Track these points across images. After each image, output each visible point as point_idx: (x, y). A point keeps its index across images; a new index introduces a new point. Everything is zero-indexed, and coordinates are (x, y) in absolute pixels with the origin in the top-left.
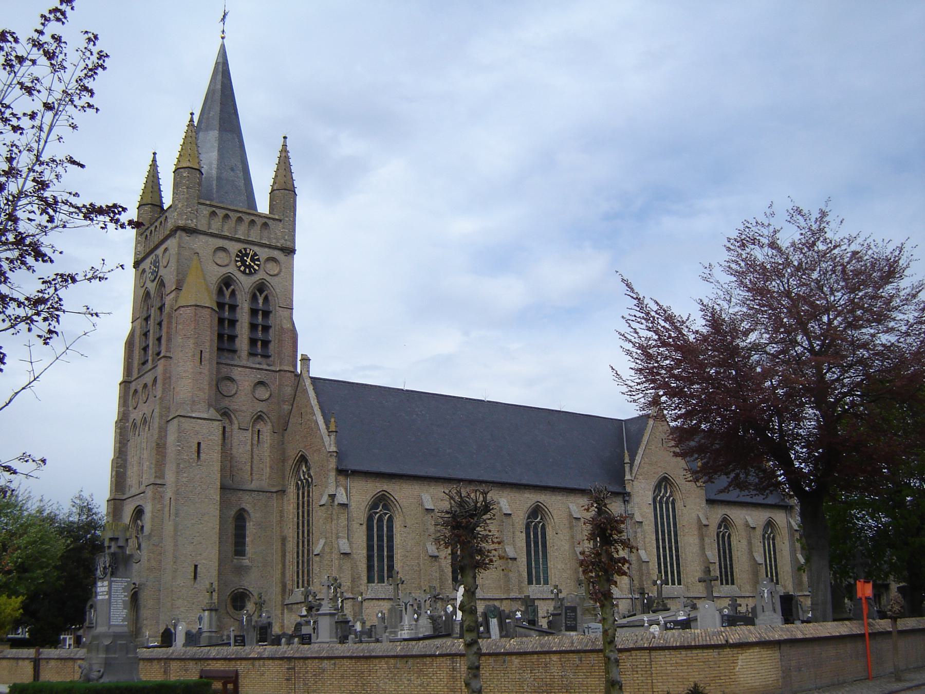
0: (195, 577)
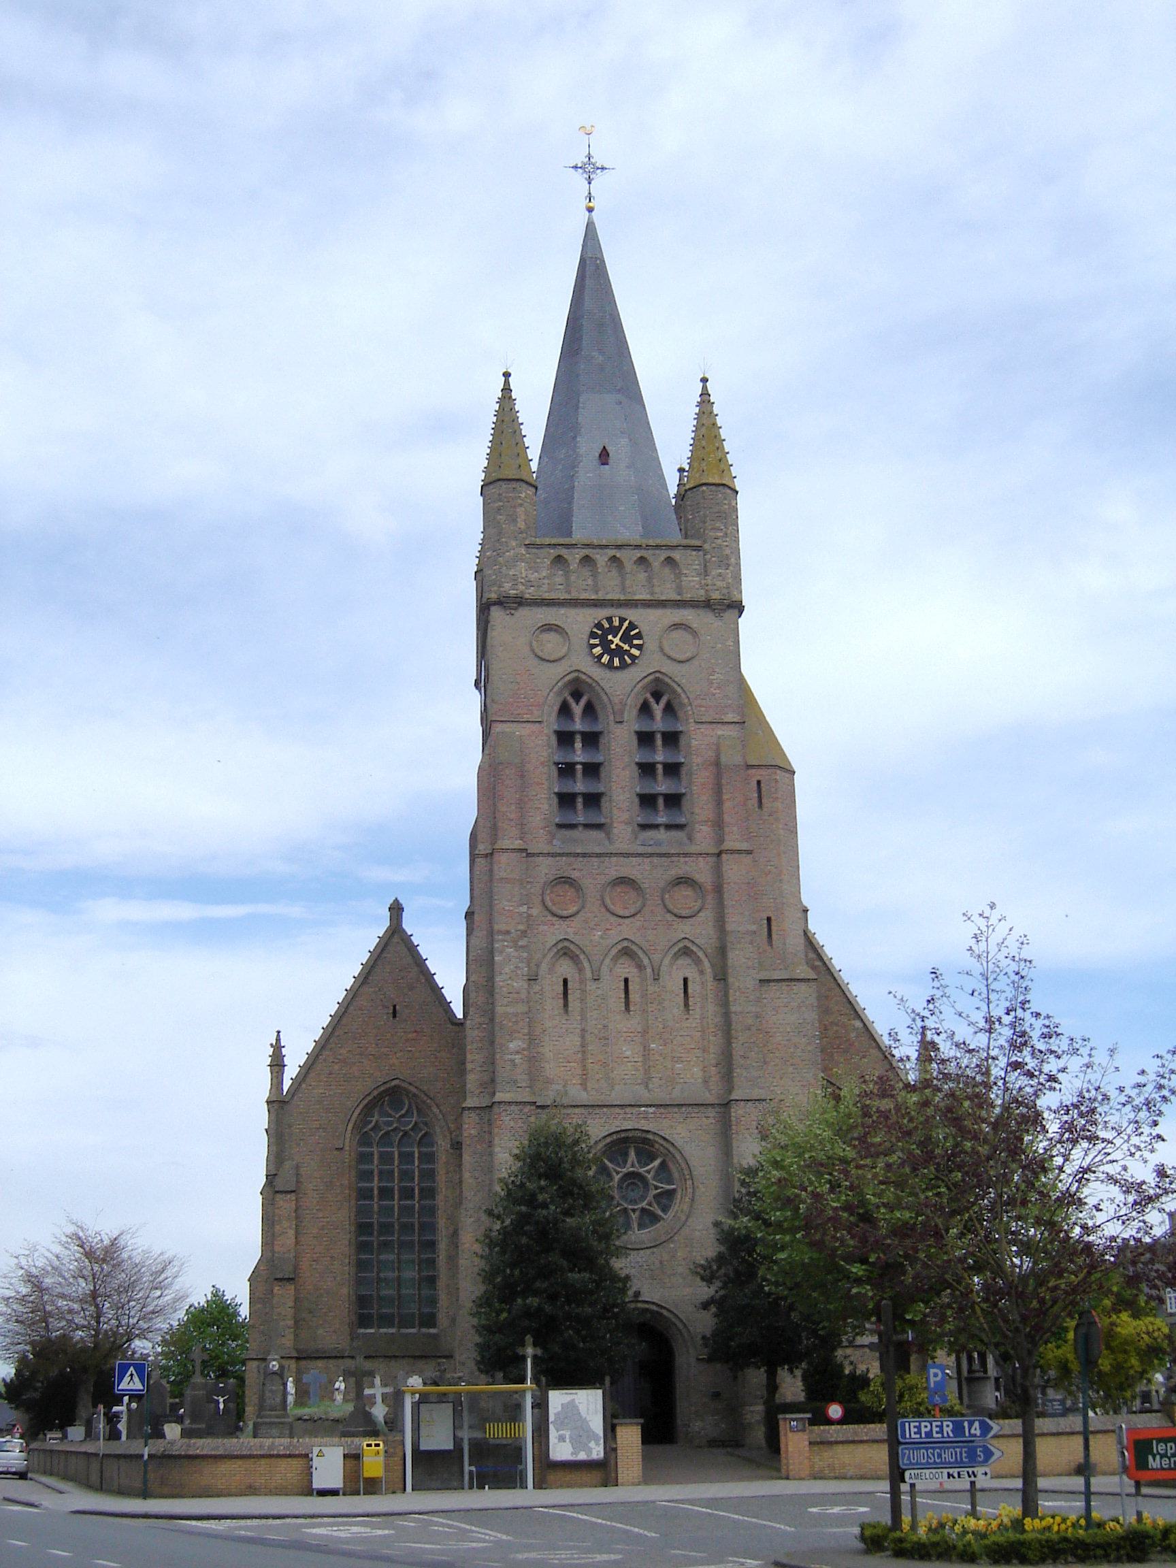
0: (686, 1005)
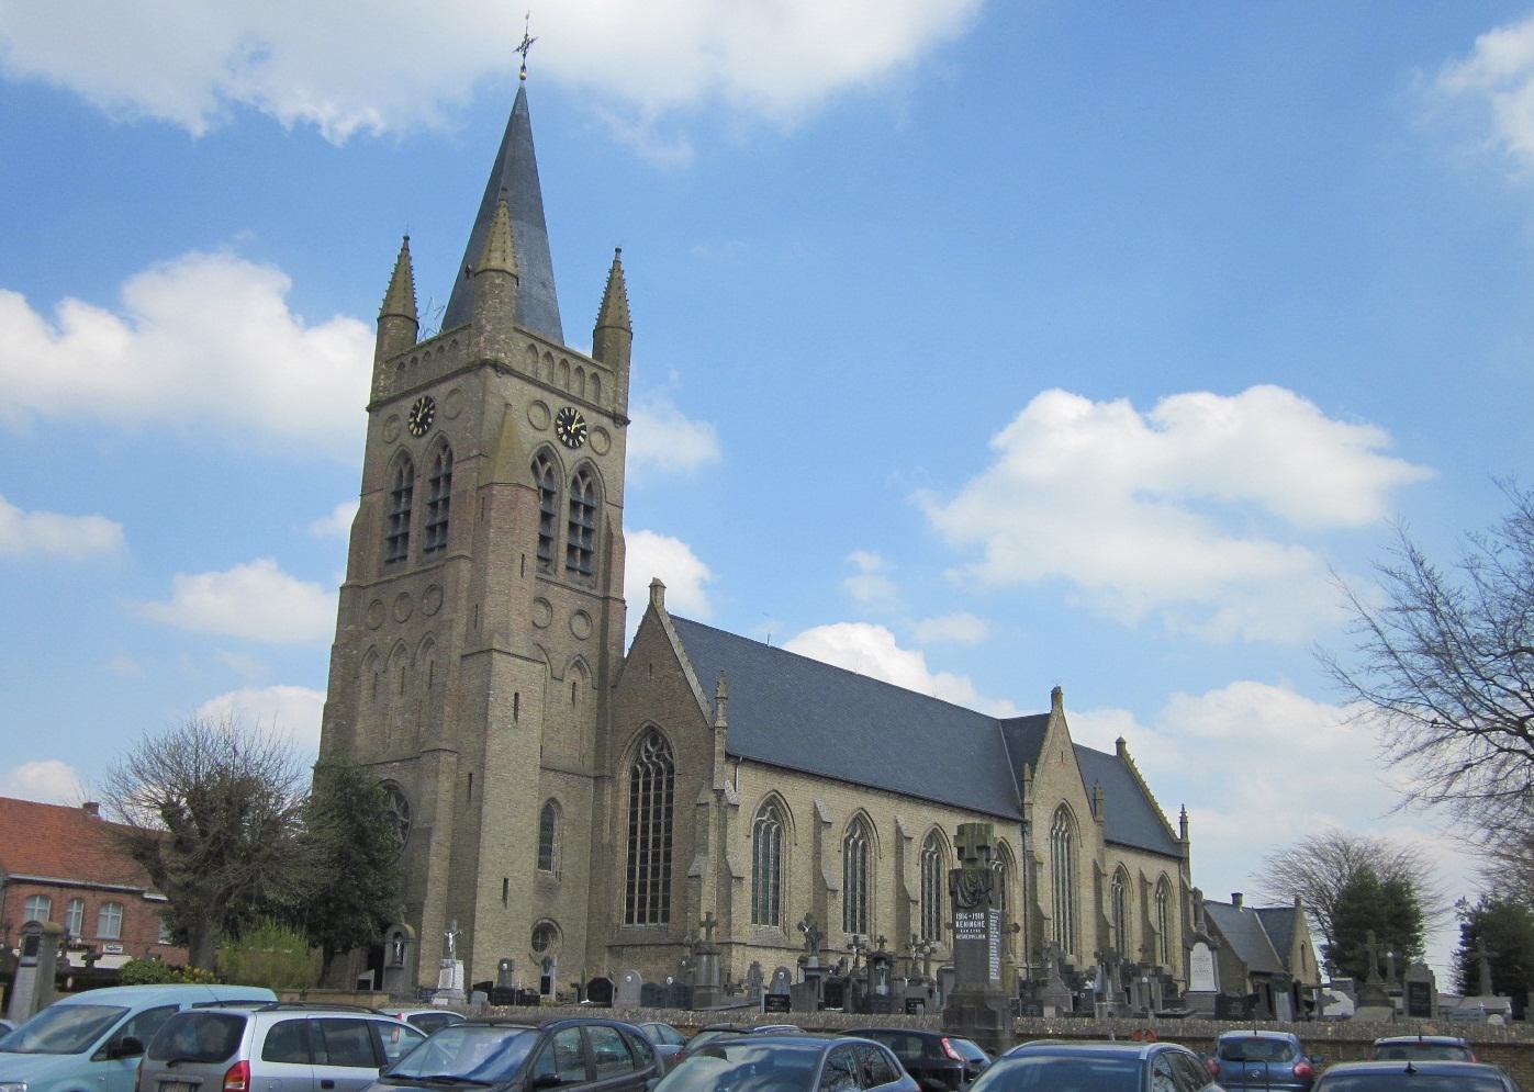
0: (505, 898)
